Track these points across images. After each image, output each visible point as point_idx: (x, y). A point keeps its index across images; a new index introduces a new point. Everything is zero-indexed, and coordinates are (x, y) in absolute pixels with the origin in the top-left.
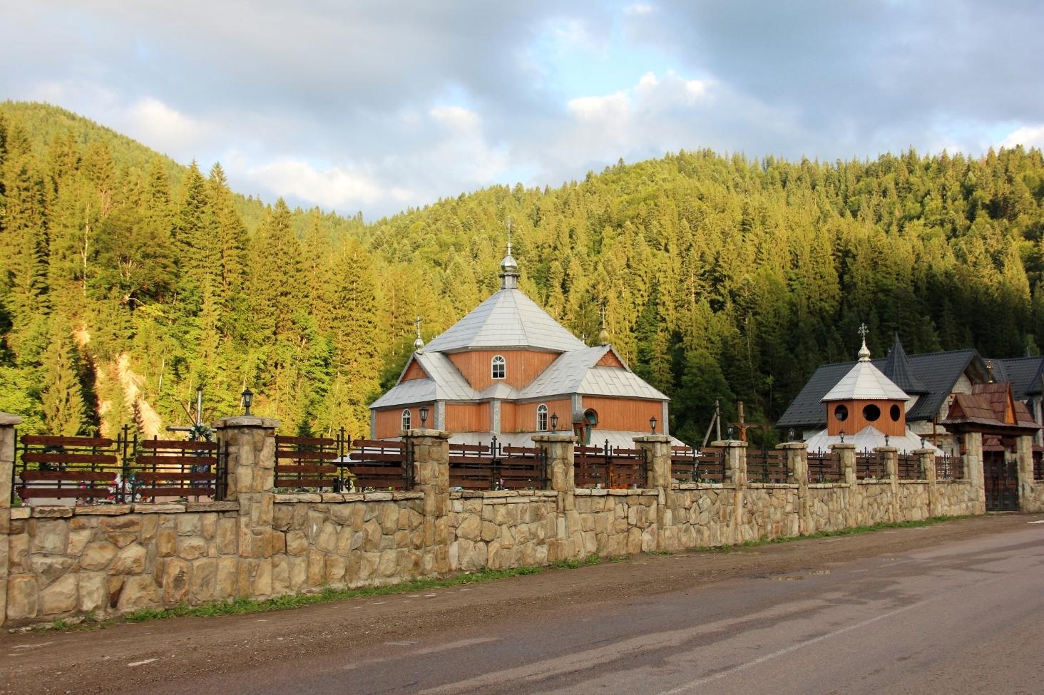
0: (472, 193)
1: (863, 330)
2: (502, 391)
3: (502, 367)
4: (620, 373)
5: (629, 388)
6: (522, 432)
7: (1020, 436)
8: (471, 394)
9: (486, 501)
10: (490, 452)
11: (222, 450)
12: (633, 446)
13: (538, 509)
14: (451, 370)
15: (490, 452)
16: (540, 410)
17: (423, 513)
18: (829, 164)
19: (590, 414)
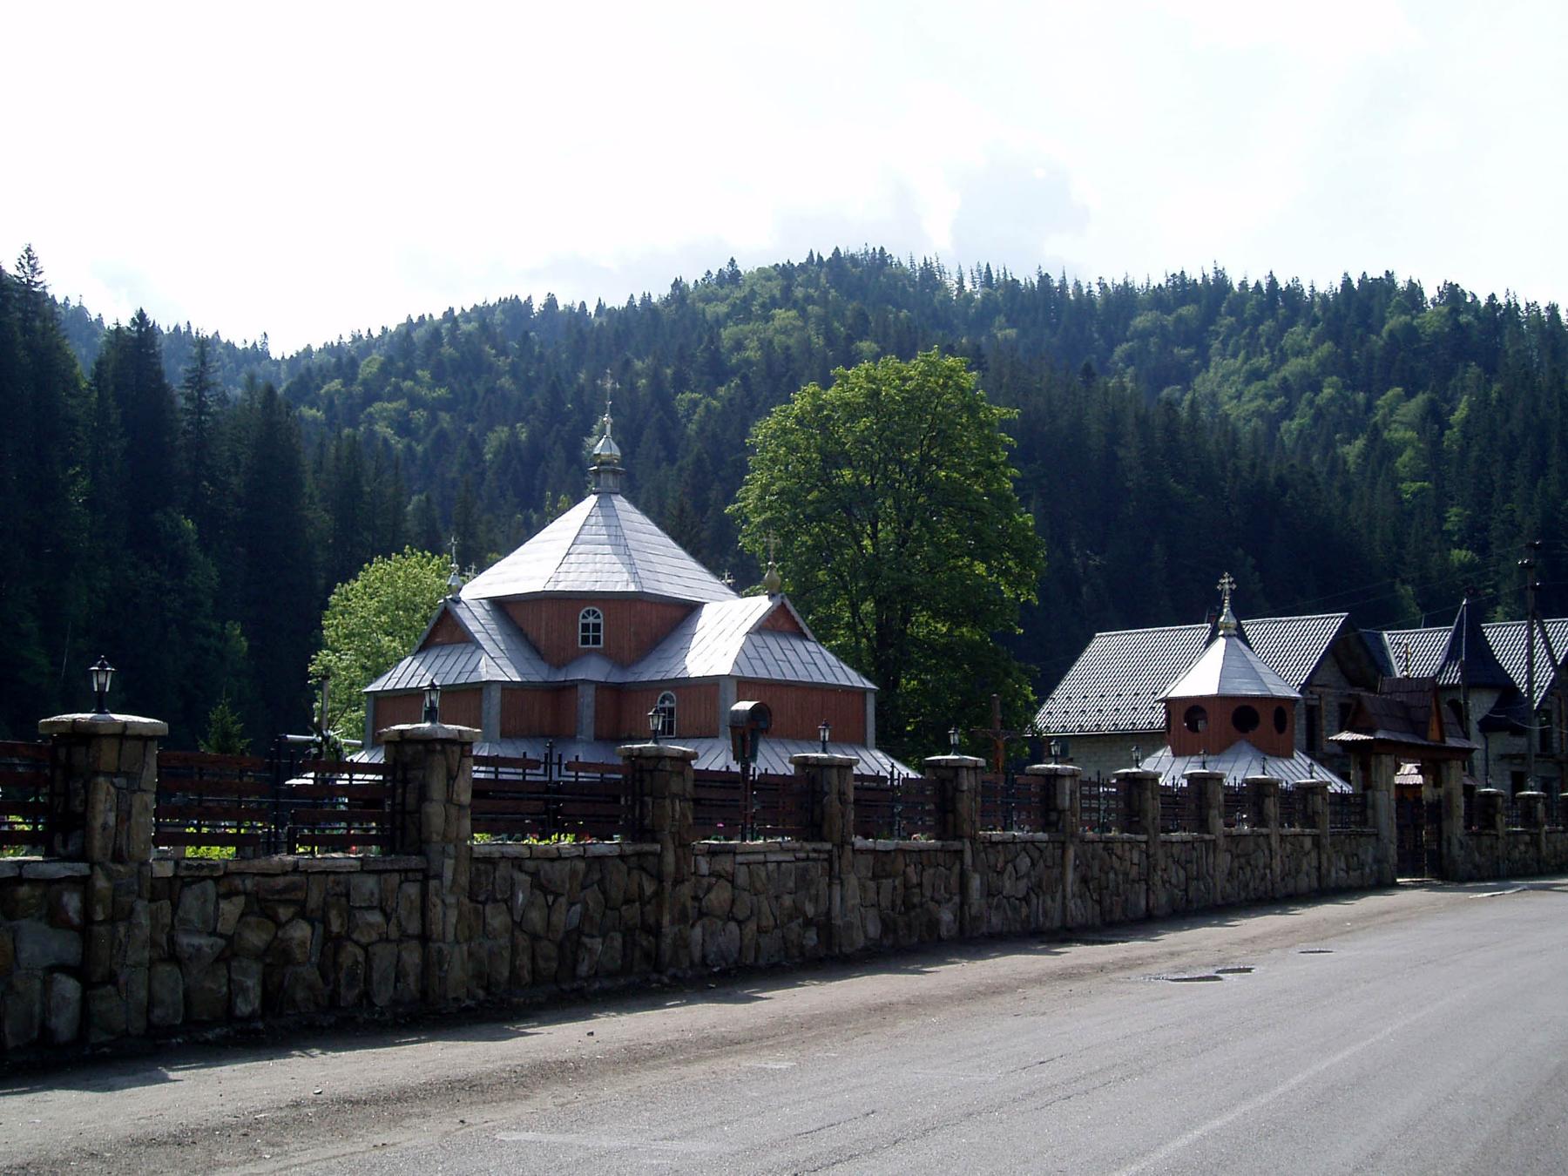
0: (468, 310)
2: (594, 670)
4: (798, 645)
5: (812, 668)
7: (1378, 754)
8: (540, 673)
9: (739, 858)
10: (541, 771)
11: (399, 774)
12: (791, 770)
13: (806, 870)
15: (541, 771)
16: (662, 702)
17: (659, 878)
18: (1084, 285)
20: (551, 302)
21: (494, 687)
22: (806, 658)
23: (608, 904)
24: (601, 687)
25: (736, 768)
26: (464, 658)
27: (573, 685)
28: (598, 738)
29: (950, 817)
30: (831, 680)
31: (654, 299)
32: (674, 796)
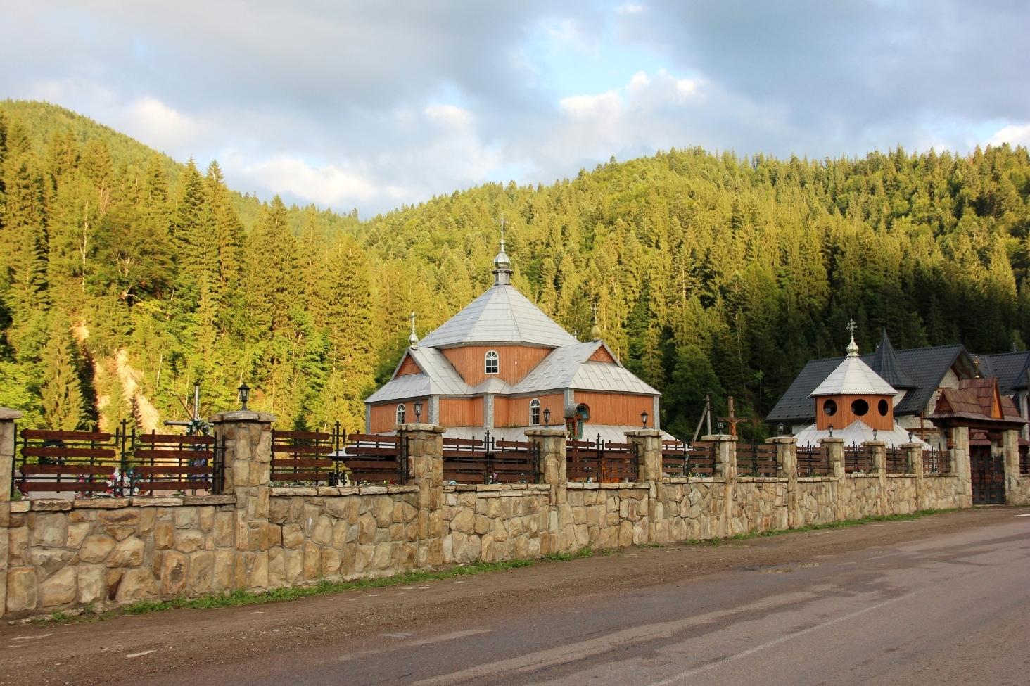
0: (466, 191)
1: (852, 325)
2: (496, 386)
3: (495, 362)
4: (611, 369)
5: (620, 383)
6: (515, 427)
7: (1006, 430)
8: (464, 389)
9: (479, 495)
10: (483, 447)
12: (624, 440)
13: (531, 502)
14: (445, 366)
15: (483, 447)
16: (532, 405)
17: (417, 507)
18: (818, 162)
19: (583, 408)
21: (844, 399)
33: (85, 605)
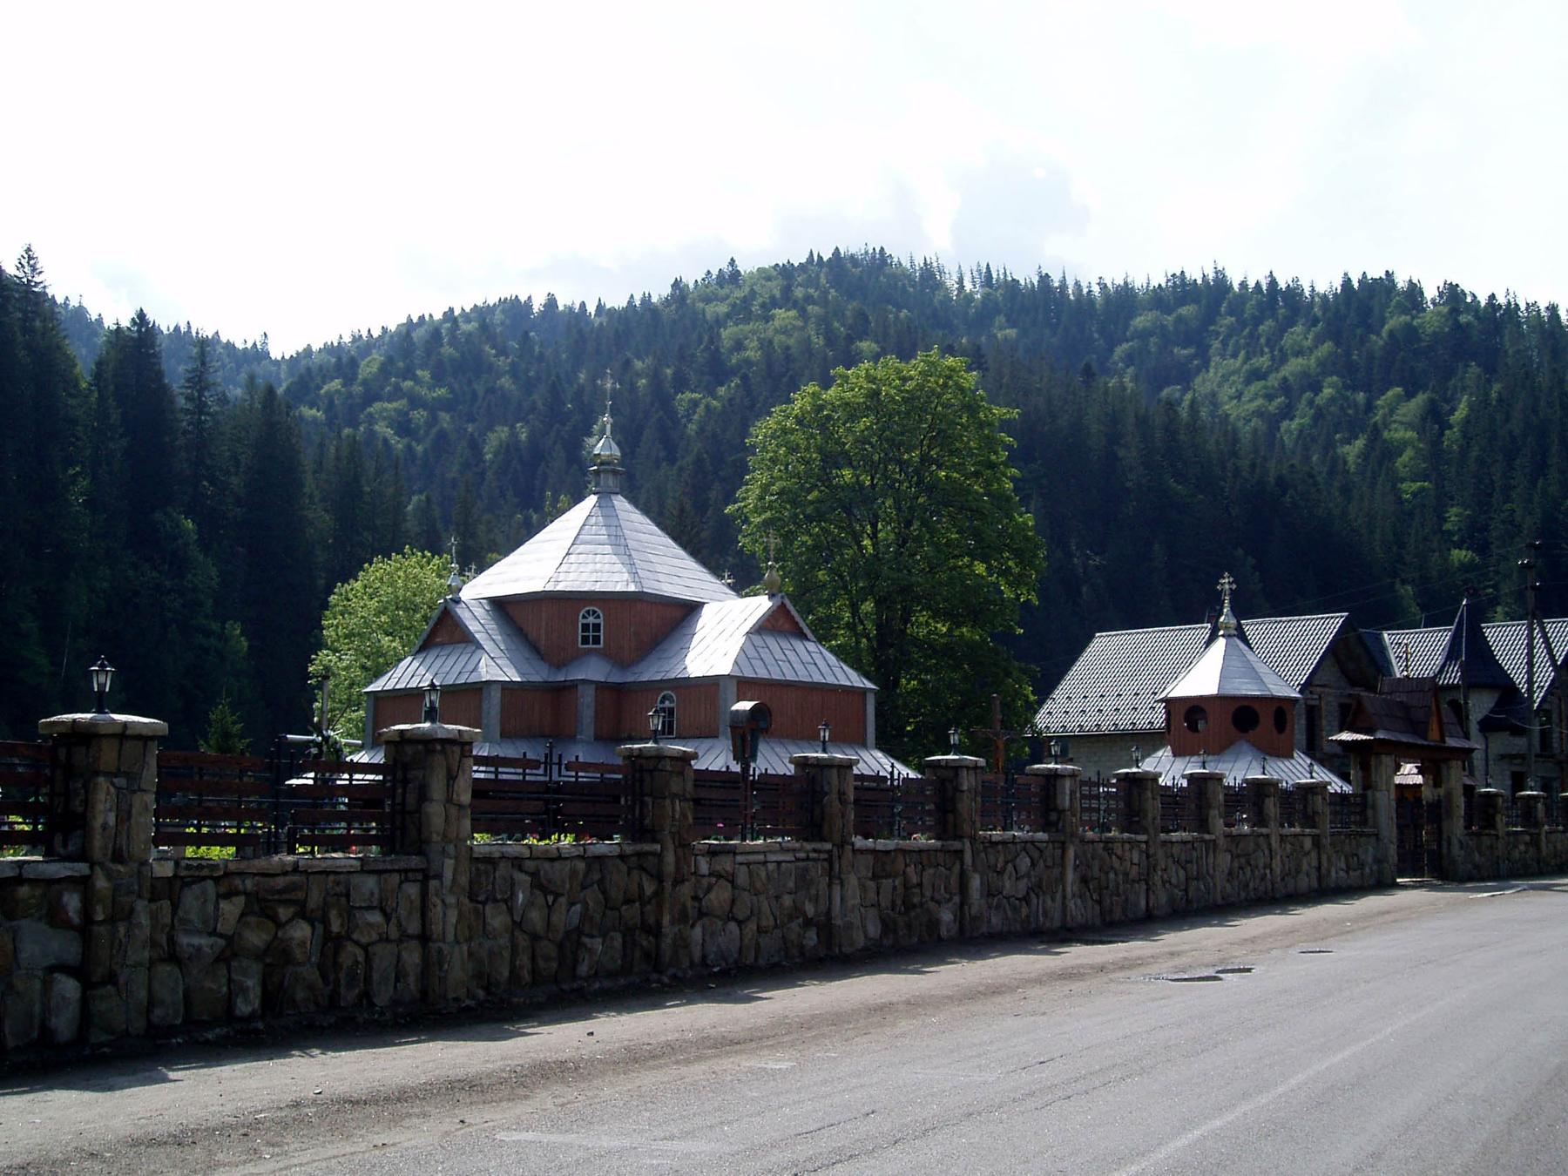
0: (468, 310)
2: (594, 670)
4: (798, 645)
5: (812, 668)
7: (1378, 754)
8: (540, 673)
9: (739, 858)
10: (541, 771)
12: (791, 770)
13: (806, 870)
15: (541, 771)
16: (662, 702)
17: (659, 878)
18: (1084, 285)
20: (551, 302)
22: (806, 658)
23: (608, 904)
24: (601, 687)
25: (736, 768)
26: (464, 658)
27: (573, 685)
28: (598, 738)
29: (950, 817)
30: (831, 680)
31: (654, 299)
32: (674, 796)
33: (241, 1019)
